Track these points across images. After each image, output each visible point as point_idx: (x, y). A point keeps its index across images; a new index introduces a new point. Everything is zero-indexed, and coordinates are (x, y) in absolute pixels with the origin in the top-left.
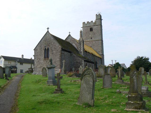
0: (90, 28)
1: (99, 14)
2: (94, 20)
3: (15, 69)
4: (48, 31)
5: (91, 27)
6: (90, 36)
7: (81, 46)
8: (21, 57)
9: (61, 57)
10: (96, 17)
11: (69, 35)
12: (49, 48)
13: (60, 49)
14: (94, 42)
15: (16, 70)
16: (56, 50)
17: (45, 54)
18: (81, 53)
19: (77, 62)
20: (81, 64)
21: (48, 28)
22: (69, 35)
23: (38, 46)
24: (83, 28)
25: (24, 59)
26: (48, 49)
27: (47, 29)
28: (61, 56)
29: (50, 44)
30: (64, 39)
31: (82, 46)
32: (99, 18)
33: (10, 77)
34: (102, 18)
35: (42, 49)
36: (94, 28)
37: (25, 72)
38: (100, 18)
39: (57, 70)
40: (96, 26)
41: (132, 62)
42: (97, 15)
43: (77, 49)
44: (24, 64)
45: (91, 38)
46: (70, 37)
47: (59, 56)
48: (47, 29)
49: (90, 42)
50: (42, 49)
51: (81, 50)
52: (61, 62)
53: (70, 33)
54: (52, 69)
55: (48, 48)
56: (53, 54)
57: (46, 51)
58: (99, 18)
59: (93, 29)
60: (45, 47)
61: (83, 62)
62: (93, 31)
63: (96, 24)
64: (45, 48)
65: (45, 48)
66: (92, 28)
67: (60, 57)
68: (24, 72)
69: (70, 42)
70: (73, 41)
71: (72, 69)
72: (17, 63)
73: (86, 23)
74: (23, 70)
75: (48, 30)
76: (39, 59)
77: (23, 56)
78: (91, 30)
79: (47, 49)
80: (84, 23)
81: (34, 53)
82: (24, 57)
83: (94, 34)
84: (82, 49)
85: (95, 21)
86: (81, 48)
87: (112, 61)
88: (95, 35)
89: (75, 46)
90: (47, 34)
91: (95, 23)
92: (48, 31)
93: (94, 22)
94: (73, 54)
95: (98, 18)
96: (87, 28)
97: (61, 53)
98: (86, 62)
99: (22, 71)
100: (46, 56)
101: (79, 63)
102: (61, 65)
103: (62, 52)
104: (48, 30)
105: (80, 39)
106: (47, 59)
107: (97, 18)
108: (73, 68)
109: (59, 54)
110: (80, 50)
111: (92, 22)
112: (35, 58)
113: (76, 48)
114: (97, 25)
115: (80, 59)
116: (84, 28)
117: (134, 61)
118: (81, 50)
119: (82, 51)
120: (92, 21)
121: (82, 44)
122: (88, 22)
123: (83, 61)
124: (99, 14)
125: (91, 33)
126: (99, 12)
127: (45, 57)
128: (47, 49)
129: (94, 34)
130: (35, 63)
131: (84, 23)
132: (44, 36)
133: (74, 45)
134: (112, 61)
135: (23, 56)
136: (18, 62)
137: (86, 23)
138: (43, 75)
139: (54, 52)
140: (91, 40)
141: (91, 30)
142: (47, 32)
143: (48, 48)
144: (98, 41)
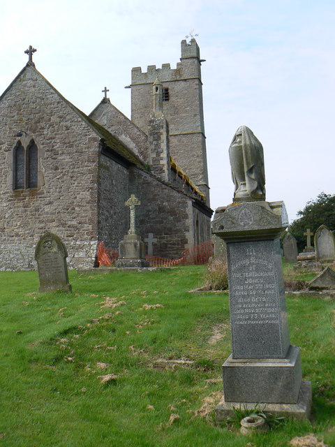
1: (193, 41)
2: (173, 57)
4: (30, 64)
5: (165, 85)
7: (158, 146)
9: (99, 184)
10: (183, 51)
11: (105, 101)
12: (38, 141)
13: (95, 147)
16: (74, 149)
17: (16, 170)
18: (162, 171)
19: (161, 209)
21: (31, 51)
22: (105, 101)
24: (135, 88)
26: (32, 145)
27: (26, 52)
28: (99, 180)
29: (43, 124)
31: (163, 146)
32: (192, 54)
35: (4, 146)
36: (175, 89)
38: (195, 55)
39: (81, 247)
40: (183, 83)
41: (300, 213)
42: (184, 42)
43: (141, 158)
46: (106, 109)
47: (87, 180)
48: (26, 52)
51: (162, 162)
52: (99, 207)
53: (106, 91)
55: (32, 142)
56: (57, 168)
57: (24, 157)
58: (192, 54)
59: (170, 92)
60: (20, 135)
62: (172, 99)
63: (181, 76)
64: (19, 143)
65: (19, 143)
67: (93, 182)
69: (109, 130)
70: (119, 123)
73: (144, 70)
78: (166, 95)
80: (136, 71)
81: (181, 53)
83: (176, 110)
84: (164, 155)
85: (178, 64)
86: (158, 154)
88: (177, 113)
89: (132, 145)
90: (28, 75)
91: (178, 71)
92: (30, 64)
93: (174, 67)
94: (140, 176)
95: (189, 55)
97: (100, 166)
100: (23, 180)
101: (172, 212)
102: (99, 222)
103: (103, 159)
106: (26, 192)
107: (186, 56)
109: (90, 172)
110: (158, 159)
111: (166, 66)
113: (136, 152)
114: (185, 80)
115: (175, 194)
116: (138, 87)
117: (307, 209)
118: (162, 162)
119: (163, 165)
121: (164, 137)
122: (152, 69)
123: (190, 203)
124: (193, 41)
126: (193, 34)
127: (16, 186)
128: (25, 144)
129: (176, 110)
131: (136, 71)
133: (125, 139)
137: (144, 70)
138: (44, 283)
139: (66, 159)
141: (166, 95)
142: (24, 69)
143: (32, 142)
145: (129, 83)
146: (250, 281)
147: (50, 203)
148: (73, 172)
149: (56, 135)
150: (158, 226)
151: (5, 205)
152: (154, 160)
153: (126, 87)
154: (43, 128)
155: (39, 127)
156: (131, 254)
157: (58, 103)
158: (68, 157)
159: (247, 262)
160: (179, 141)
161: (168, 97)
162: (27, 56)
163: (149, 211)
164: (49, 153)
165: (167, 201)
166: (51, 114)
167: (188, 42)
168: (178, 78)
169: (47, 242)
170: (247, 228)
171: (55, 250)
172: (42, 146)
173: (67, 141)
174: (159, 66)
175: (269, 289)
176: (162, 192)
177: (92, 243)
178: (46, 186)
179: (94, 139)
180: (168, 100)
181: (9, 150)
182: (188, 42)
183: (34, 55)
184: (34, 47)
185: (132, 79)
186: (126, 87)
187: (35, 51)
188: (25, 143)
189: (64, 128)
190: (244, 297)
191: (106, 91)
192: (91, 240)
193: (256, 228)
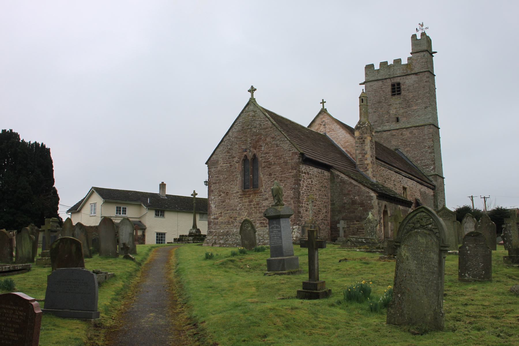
0: (393, 85)
3: (140, 233)
5: (397, 80)
6: (393, 112)
8: (156, 190)
10: (413, 45)
11: (323, 111)
12: (259, 156)
14: (407, 133)
15: (144, 235)
19: (354, 202)
20: (367, 208)
22: (323, 111)
23: (218, 150)
24: (368, 84)
25: (167, 196)
26: (255, 158)
30: (306, 125)
33: (134, 252)
34: (93, 225)
35: (236, 159)
36: (408, 82)
37: (175, 240)
38: (425, 47)
40: (413, 77)
44: (167, 214)
45: (398, 120)
49: (394, 133)
50: (236, 159)
51: (366, 162)
53: (323, 102)
54: (415, 51)
55: (255, 155)
61: (375, 201)
62: (403, 93)
64: (246, 156)
65: (246, 156)
66: (399, 84)
68: (169, 238)
71: (338, 225)
72: (144, 210)
73: (377, 67)
74: (164, 234)
75: (252, 95)
76: (223, 195)
77: (163, 186)
78: (396, 89)
79: (249, 158)
80: (369, 68)
82: (169, 191)
85: (409, 59)
87: (472, 200)
88: (409, 107)
93: (404, 62)
96: (380, 83)
98: (384, 203)
99: (160, 237)
101: (362, 204)
104: (252, 95)
105: (359, 123)
108: (342, 222)
111: (398, 61)
112: (212, 191)
114: (416, 74)
120: (400, 60)
122: (384, 64)
125: (396, 101)
130: (213, 206)
131: (369, 68)
132: (240, 115)
134: (472, 200)
135: (163, 186)
136: (150, 207)
137: (377, 67)
140: (398, 126)
141: (396, 89)
143: (255, 155)
144: (422, 127)
145: (363, 80)
146: (274, 232)
147: (267, 199)
148: (281, 177)
149: (270, 150)
150: (352, 215)
151: (237, 201)
152: (361, 160)
153: (361, 84)
154: (261, 146)
155: (259, 145)
156: (160, 215)
157: (271, 128)
158: (278, 166)
159: (273, 226)
160: (411, 133)
161: (400, 91)
162: (250, 94)
163: (345, 203)
164: (266, 164)
165: (358, 196)
166: (266, 136)
167: (419, 37)
168: (409, 72)
169: (245, 224)
170: (272, 215)
171: (249, 228)
172: (261, 159)
173: (277, 154)
174: (390, 62)
175: (279, 234)
176: (354, 188)
177: (294, 227)
178: (264, 187)
179: (296, 153)
180: (400, 94)
181: (239, 162)
182: (419, 37)
183: (255, 93)
184: (255, 87)
185: (366, 76)
186: (361, 84)
187: (255, 90)
188: (250, 156)
189: (275, 146)
190: (273, 237)
191: (323, 102)
192: (293, 225)
193: (274, 214)
